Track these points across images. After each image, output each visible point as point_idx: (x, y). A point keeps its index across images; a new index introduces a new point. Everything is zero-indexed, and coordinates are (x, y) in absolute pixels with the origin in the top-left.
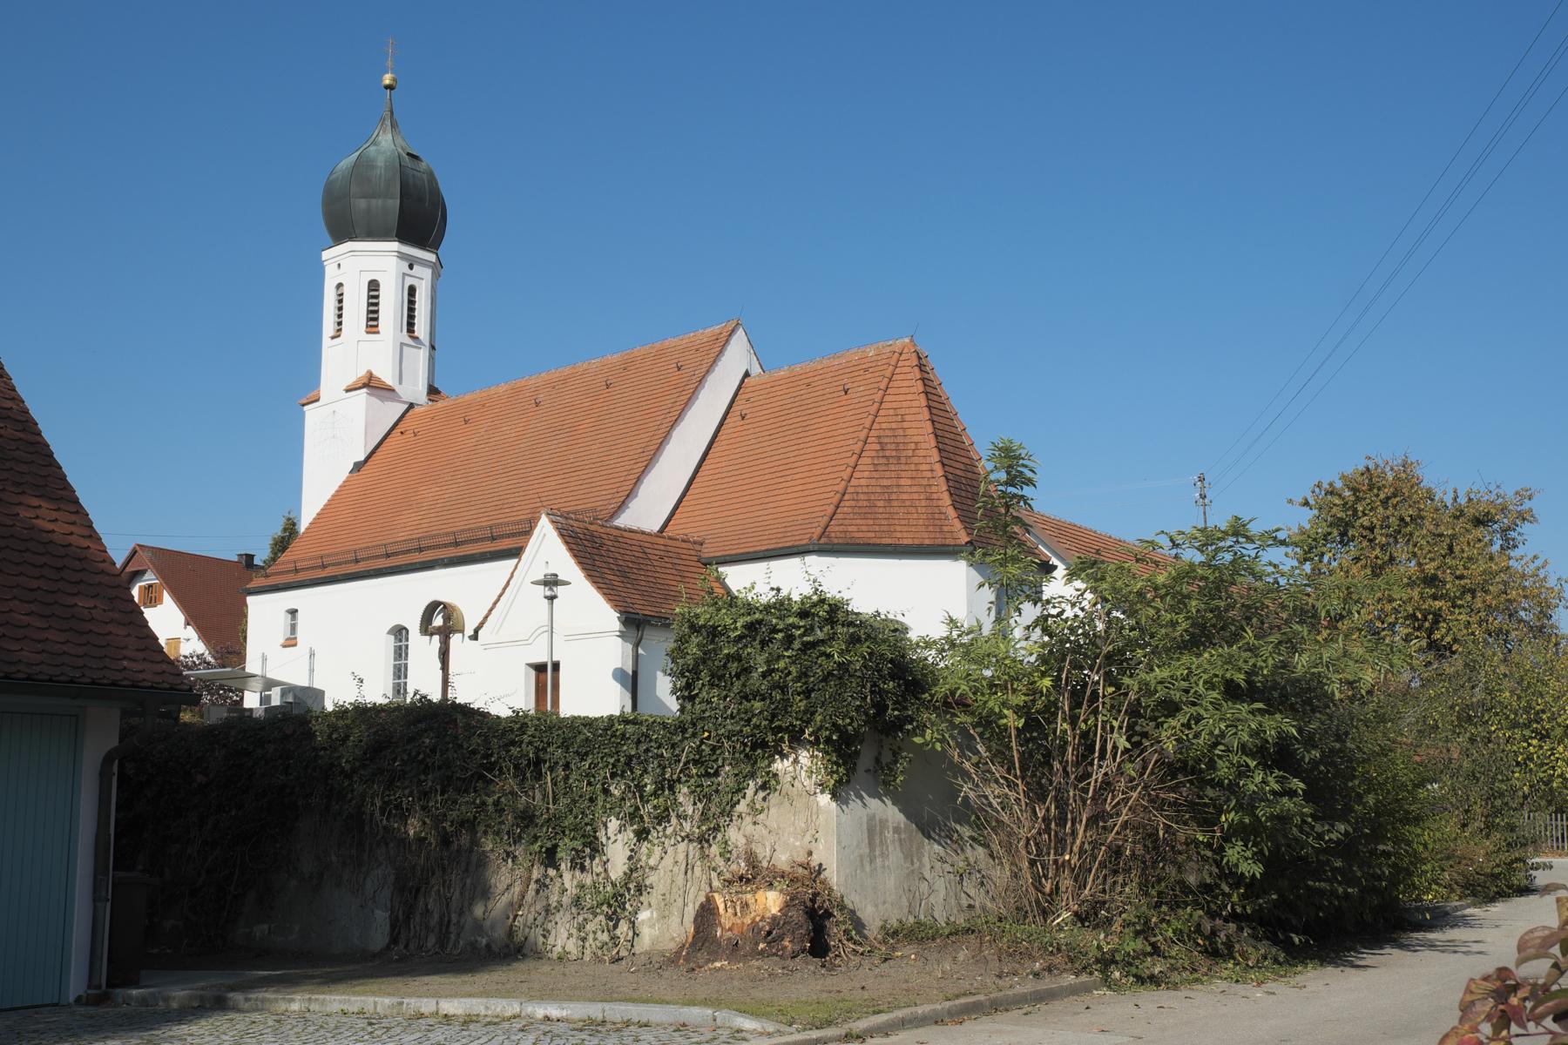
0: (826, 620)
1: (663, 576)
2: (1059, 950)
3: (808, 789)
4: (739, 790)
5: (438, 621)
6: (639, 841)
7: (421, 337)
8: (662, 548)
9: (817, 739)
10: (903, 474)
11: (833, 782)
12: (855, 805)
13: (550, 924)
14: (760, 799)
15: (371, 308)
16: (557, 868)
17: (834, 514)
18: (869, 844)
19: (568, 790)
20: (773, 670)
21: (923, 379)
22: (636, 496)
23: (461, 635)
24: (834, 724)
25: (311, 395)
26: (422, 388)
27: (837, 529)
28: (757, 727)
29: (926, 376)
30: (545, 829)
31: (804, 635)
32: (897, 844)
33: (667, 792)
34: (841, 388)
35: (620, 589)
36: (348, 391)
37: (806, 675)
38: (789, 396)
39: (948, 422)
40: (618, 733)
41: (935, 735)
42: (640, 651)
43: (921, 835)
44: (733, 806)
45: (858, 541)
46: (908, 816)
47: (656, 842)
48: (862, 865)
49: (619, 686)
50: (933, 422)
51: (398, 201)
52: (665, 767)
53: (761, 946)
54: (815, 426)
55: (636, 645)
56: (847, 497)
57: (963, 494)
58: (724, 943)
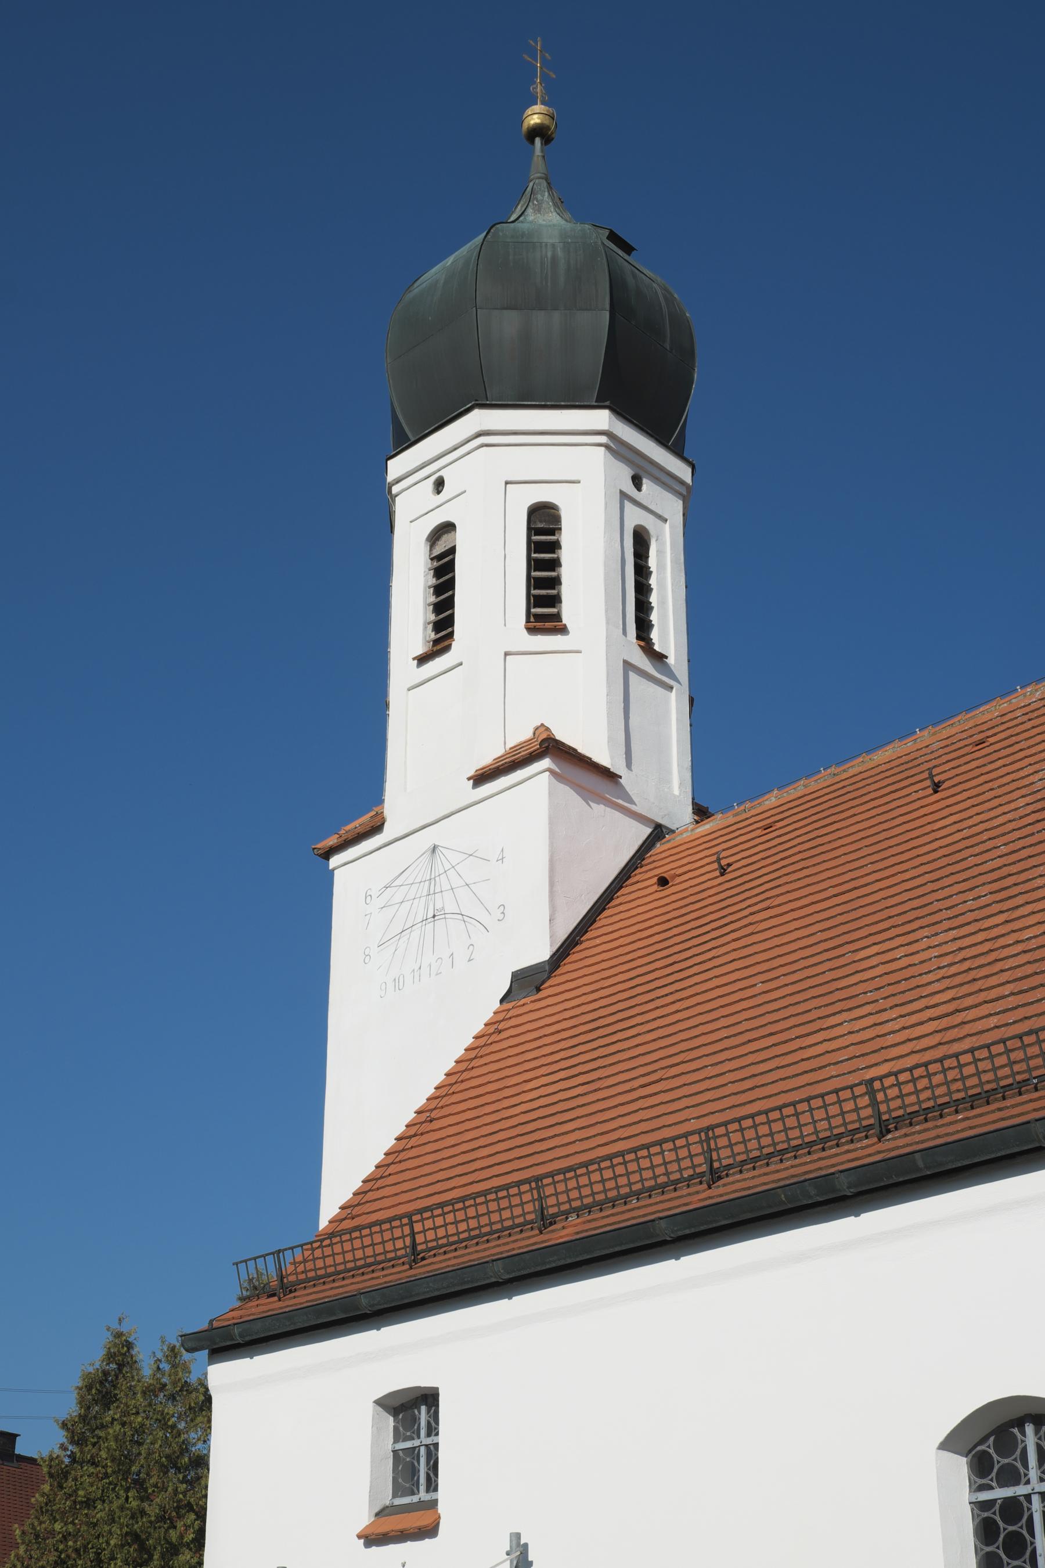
7: (671, 661)
36: (481, 778)
51: (606, 315)
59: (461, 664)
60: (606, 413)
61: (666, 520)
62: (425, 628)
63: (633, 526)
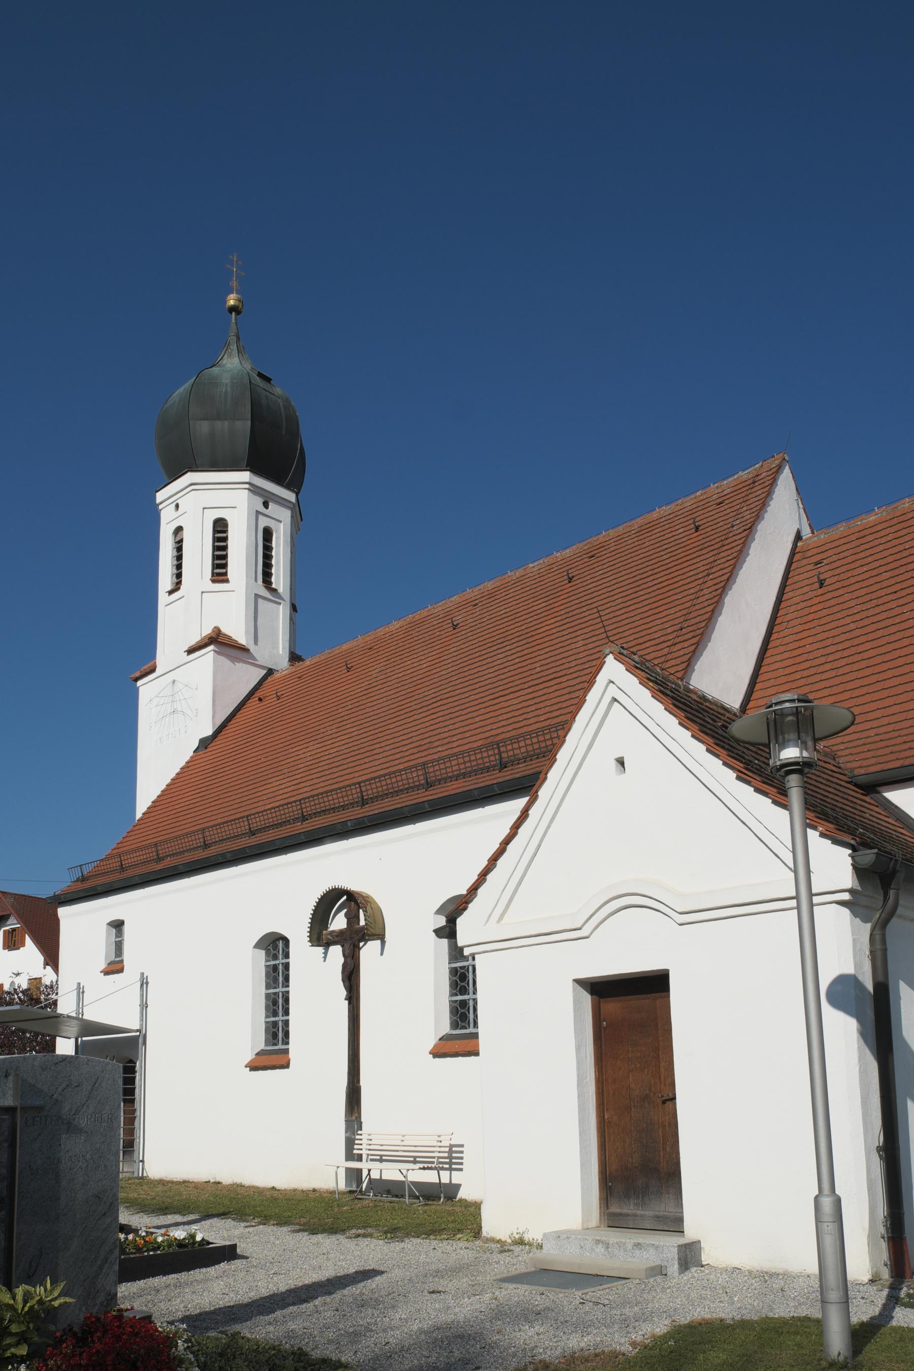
5: (339, 922)
7: (281, 590)
25: (146, 667)
36: (190, 651)
51: (249, 422)
59: (183, 597)
61: (281, 522)
62: (172, 577)
63: (263, 527)
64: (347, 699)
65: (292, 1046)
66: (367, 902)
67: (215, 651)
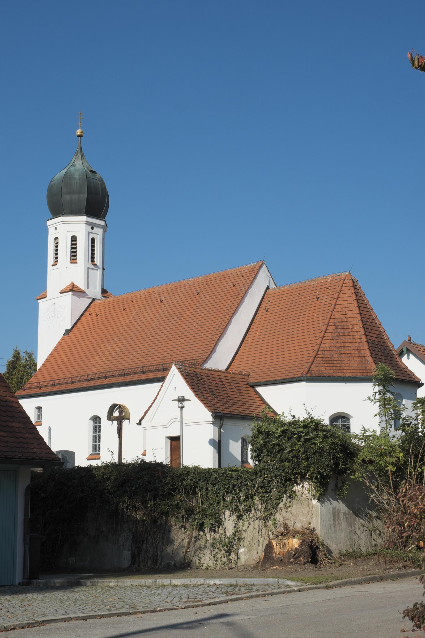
0: (314, 429)
1: (231, 393)
2: (409, 560)
3: (308, 497)
4: (280, 498)
5: (116, 414)
6: (238, 520)
7: (98, 264)
8: (230, 378)
9: (312, 477)
10: (347, 341)
11: (318, 495)
12: (327, 503)
13: (201, 555)
14: (289, 502)
15: (73, 250)
16: (204, 532)
17: (314, 361)
18: (334, 519)
19: (208, 499)
20: (293, 450)
21: (355, 293)
22: (215, 352)
23: (128, 420)
24: (318, 472)
26: (98, 290)
27: (315, 369)
28: (287, 473)
29: (357, 291)
30: (198, 515)
31: (305, 436)
32: (345, 519)
33: (250, 500)
34: (315, 297)
35: (211, 401)
36: (61, 293)
37: (307, 452)
38: (289, 300)
39: (368, 313)
40: (229, 475)
41: (359, 475)
42: (222, 431)
43: (355, 516)
44: (278, 505)
45: (325, 375)
46: (349, 508)
47: (246, 520)
48: (331, 528)
49: (212, 448)
50: (361, 314)
51: (86, 195)
52: (248, 490)
53: (292, 560)
54: (303, 316)
55: (220, 428)
56: (319, 353)
57: (376, 350)
58: (276, 559)
60: (85, 217)
61: (98, 234)
64: (123, 325)
65: (101, 452)
66: (125, 408)
67: (72, 294)
